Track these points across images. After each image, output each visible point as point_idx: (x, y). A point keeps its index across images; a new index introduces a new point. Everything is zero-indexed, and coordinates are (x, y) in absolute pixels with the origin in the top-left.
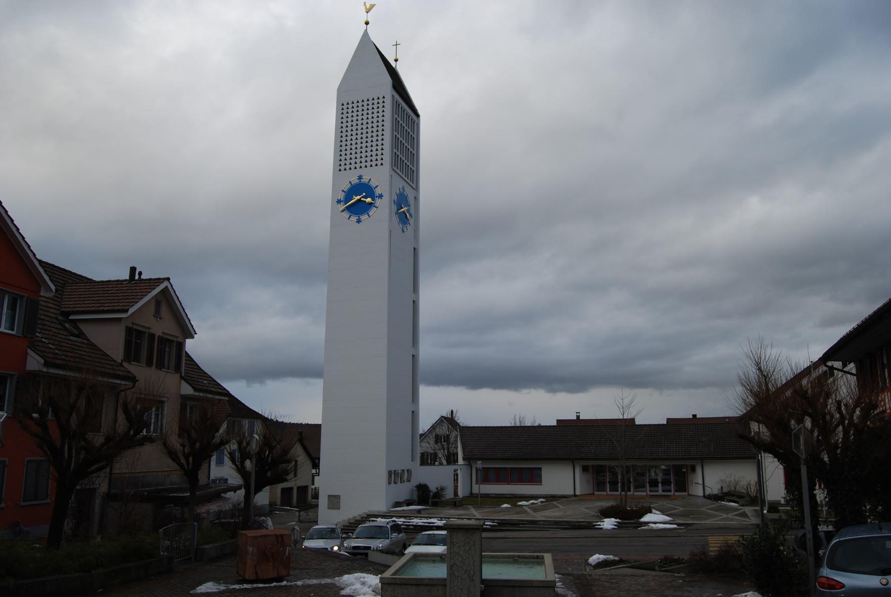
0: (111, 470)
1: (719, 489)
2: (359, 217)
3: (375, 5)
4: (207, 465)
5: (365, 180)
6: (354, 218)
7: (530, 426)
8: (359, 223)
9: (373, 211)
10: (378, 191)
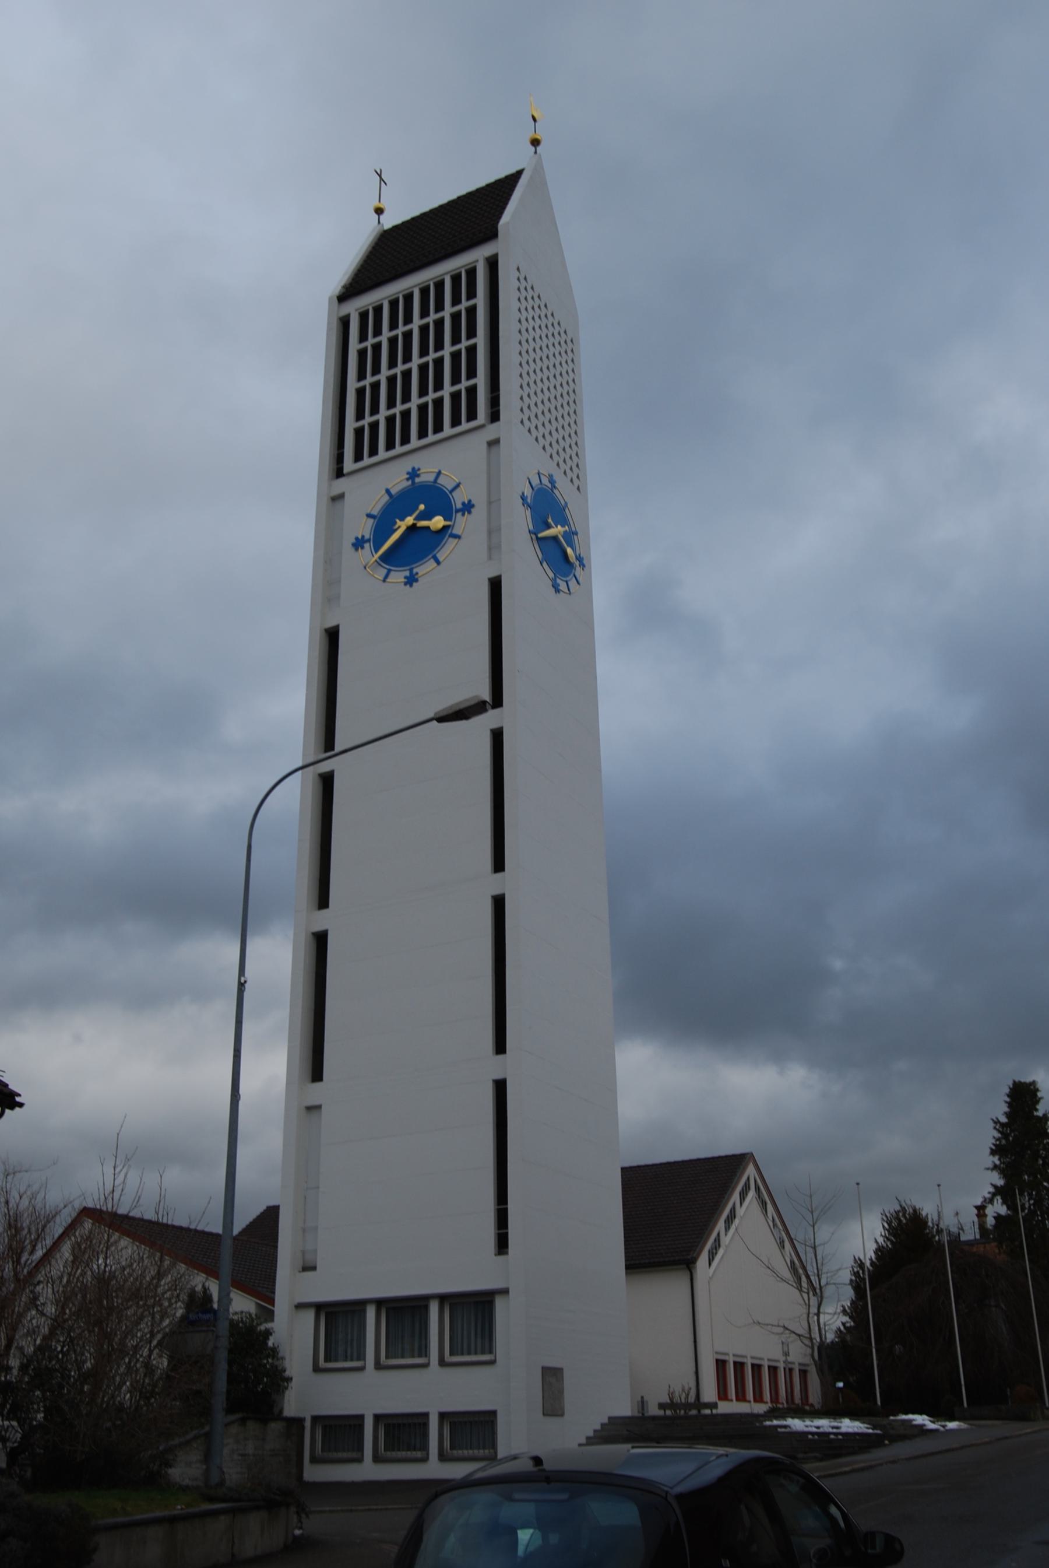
0: (6, 1450)
1: (638, 1402)
2: (411, 570)
3: (519, 174)
4: (529, 1550)
5: (426, 477)
6: (398, 576)
7: (181, 1228)
8: (411, 586)
9: (447, 550)
10: (459, 498)
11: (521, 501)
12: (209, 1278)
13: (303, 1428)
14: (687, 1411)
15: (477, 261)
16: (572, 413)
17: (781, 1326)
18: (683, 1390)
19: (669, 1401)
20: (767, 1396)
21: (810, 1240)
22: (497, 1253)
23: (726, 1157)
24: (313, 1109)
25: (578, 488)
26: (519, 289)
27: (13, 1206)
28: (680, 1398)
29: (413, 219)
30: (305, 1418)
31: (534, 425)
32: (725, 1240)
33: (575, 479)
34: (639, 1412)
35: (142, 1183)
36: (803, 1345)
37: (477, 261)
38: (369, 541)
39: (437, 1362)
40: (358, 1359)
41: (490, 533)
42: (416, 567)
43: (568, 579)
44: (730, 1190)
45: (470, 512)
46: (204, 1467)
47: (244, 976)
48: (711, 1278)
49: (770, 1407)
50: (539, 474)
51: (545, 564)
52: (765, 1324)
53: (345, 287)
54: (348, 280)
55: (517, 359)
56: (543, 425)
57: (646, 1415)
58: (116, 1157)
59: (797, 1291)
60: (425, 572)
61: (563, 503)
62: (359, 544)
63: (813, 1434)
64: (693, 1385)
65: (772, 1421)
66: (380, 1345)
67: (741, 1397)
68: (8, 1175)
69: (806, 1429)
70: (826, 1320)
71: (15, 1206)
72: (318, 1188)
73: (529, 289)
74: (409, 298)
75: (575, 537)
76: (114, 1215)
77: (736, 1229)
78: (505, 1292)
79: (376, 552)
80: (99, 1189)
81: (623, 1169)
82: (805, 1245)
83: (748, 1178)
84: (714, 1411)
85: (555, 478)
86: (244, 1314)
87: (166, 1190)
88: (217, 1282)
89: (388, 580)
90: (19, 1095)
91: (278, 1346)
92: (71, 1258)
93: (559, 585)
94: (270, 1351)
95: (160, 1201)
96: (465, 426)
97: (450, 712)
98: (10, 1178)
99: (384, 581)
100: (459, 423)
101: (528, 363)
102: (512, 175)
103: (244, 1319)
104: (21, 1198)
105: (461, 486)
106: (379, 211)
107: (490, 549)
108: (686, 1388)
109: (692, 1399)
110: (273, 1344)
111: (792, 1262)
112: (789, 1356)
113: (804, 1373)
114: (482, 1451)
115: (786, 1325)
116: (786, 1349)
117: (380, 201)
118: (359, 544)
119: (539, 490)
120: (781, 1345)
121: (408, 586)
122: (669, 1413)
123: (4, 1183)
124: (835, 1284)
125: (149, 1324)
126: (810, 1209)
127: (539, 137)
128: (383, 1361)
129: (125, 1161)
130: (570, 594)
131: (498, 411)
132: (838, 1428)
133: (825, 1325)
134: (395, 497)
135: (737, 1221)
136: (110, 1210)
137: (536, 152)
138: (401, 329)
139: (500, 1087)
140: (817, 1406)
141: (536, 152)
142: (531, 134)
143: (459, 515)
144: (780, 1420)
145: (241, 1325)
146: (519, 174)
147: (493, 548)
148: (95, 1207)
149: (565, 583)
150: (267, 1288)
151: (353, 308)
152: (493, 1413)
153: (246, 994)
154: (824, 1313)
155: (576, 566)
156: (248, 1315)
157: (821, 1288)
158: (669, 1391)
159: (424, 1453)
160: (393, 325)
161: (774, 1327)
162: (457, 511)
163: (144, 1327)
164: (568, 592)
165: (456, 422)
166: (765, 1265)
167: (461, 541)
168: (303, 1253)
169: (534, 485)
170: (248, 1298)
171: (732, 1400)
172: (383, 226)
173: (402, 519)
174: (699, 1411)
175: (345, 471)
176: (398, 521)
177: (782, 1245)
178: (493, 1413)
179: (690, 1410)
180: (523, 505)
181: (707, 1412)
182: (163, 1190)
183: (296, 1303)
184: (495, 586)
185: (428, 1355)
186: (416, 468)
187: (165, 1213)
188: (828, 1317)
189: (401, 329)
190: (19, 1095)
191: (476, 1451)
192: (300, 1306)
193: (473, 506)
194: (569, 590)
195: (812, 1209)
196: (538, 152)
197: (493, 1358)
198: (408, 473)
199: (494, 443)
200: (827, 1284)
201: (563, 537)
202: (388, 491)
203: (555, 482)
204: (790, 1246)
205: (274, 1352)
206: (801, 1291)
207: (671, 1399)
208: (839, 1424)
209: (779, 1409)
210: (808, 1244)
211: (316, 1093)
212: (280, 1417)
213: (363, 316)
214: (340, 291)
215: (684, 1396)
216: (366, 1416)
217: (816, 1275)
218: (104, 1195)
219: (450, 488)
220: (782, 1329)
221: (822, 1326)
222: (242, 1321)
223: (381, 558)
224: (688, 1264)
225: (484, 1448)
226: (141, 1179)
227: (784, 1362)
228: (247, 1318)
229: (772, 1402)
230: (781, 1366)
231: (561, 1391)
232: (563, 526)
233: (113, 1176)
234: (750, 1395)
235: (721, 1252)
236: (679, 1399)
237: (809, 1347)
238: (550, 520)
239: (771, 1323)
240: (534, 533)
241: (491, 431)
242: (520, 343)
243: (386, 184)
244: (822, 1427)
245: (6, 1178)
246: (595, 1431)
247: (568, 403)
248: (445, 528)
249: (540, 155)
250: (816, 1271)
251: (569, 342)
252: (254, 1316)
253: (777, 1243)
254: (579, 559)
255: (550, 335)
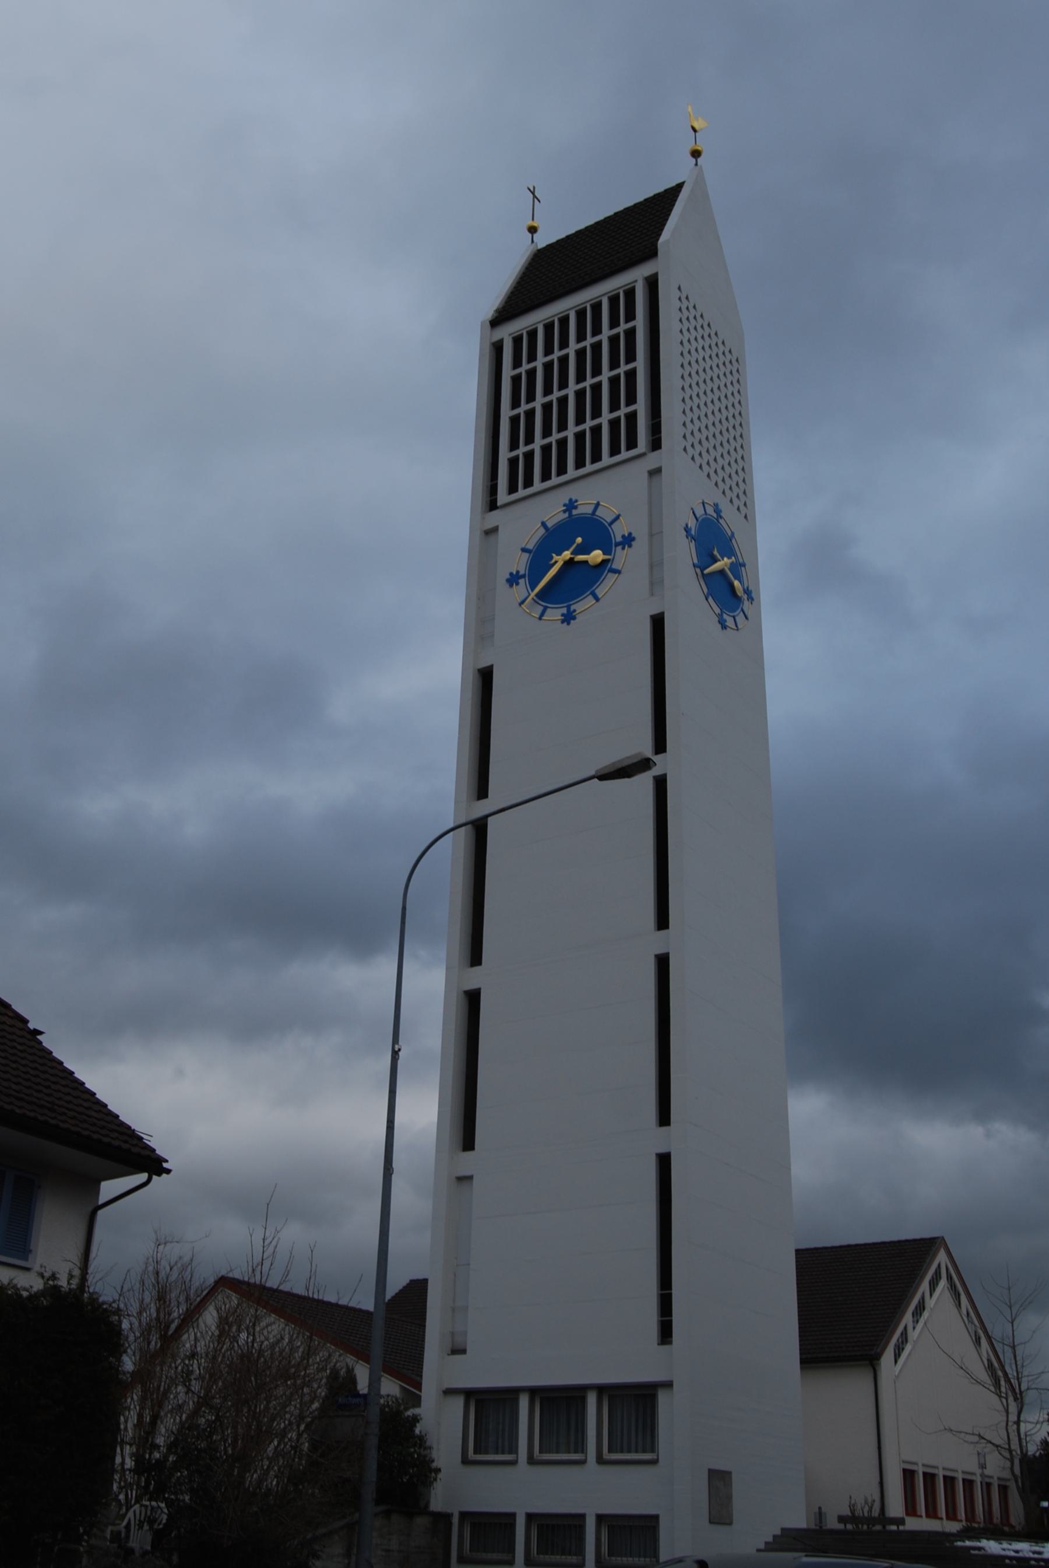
1: (815, 1513)
2: (568, 607)
3: (679, 187)
5: (584, 509)
6: (555, 614)
8: (568, 624)
9: (606, 586)
10: (618, 531)
11: (685, 533)
12: (360, 1361)
13: (451, 1524)
14: (870, 1526)
15: (636, 281)
16: (735, 382)
17: (976, 1435)
18: (866, 1502)
19: (850, 1514)
20: (962, 1513)
21: (1009, 1339)
22: (660, 1343)
23: (915, 1240)
24: (464, 1180)
25: (746, 517)
26: (680, 309)
27: (162, 1278)
28: (862, 1511)
29: (568, 237)
30: (452, 1514)
31: (698, 452)
32: (913, 1335)
33: (742, 508)
34: (816, 1525)
35: (292, 1256)
36: (1000, 1457)
37: (636, 281)
38: (523, 576)
39: (595, 1460)
40: (510, 1453)
41: (652, 567)
42: (574, 604)
43: (735, 614)
44: (919, 1278)
45: (630, 546)
46: (346, 1561)
47: (398, 1043)
48: (897, 1377)
49: (963, 1526)
50: (703, 503)
51: (710, 599)
52: (957, 1432)
53: (497, 311)
54: (500, 304)
55: (679, 407)
56: (708, 451)
57: (824, 1528)
58: (265, 1229)
59: (996, 1397)
60: (583, 609)
61: (730, 533)
62: (513, 580)
63: (1011, 1558)
64: (877, 1497)
65: (964, 1541)
66: (534, 1440)
67: (932, 1513)
68: (159, 1245)
69: (1003, 1553)
70: (1027, 1429)
71: (165, 1278)
72: (469, 1265)
73: (691, 308)
74: (564, 321)
75: (743, 568)
76: (263, 1288)
77: (925, 1323)
78: (668, 1385)
79: (532, 590)
80: (248, 1262)
81: (798, 1252)
82: (1004, 1344)
83: (939, 1265)
84: (901, 1528)
85: (721, 507)
86: (390, 1398)
87: (316, 1266)
88: (368, 1366)
89: (544, 618)
90: (167, 1161)
91: (426, 1435)
92: (217, 1333)
93: (726, 621)
94: (416, 1439)
95: (310, 1278)
96: (624, 455)
97: (612, 770)
98: (161, 1248)
99: (540, 618)
100: (619, 452)
101: (690, 363)
102: (672, 189)
103: (390, 1403)
104: (171, 1269)
105: (621, 518)
106: (533, 230)
107: (652, 584)
108: (870, 1501)
109: (876, 1513)
110: (420, 1432)
111: (989, 1360)
112: (986, 1468)
113: (1003, 1489)
114: (642, 1559)
115: (981, 1434)
116: (982, 1461)
117: (533, 219)
118: (513, 580)
119: (703, 520)
120: (976, 1457)
121: (565, 624)
122: (849, 1527)
123: (155, 1253)
124: (1037, 1389)
125: (298, 1406)
126: (1008, 1304)
127: (699, 148)
128: (537, 1456)
129: (275, 1233)
130: (738, 630)
131: (660, 439)
132: (1039, 1553)
133: (1026, 1436)
134: (551, 529)
135: (926, 1314)
136: (258, 1282)
137: (696, 164)
138: (557, 354)
139: (664, 1162)
140: (1018, 1528)
141: (696, 164)
142: (690, 146)
143: (619, 548)
144: (973, 1541)
145: (387, 1409)
146: (679, 187)
147: (655, 584)
148: (242, 1279)
149: (732, 619)
150: (413, 1370)
151: (506, 332)
152: (655, 1518)
153: (400, 1062)
154: (1025, 1422)
155: (744, 599)
156: (394, 1399)
157: (1021, 1393)
158: (850, 1503)
159: (580, 1558)
160: (549, 350)
161: (967, 1436)
162: (617, 544)
163: (293, 1408)
164: (735, 628)
165: (615, 450)
166: (958, 1365)
167: (621, 575)
168: (453, 1334)
169: (698, 516)
170: (387, 1378)
171: (921, 1516)
172: (537, 244)
173: (559, 554)
174: (884, 1527)
175: (499, 504)
176: (554, 555)
177: (977, 1341)
178: (655, 1518)
179: (874, 1525)
180: (687, 537)
181: (894, 1528)
182: (314, 1265)
183: (444, 1389)
184: (658, 623)
185: (585, 1452)
186: (574, 499)
187: (316, 1290)
188: (1029, 1426)
189: (557, 354)
190: (167, 1161)
191: (636, 1559)
192: (449, 1392)
193: (634, 539)
194: (736, 626)
195: (1010, 1303)
196: (699, 163)
197: (655, 1457)
198: (565, 505)
199: (655, 472)
200: (1028, 1389)
201: (729, 569)
202: (543, 524)
203: (721, 511)
204: (987, 1343)
205: (421, 1441)
206: (1000, 1397)
207: (853, 1512)
208: (1041, 1549)
209: (974, 1528)
210: (1005, 1342)
211: (467, 1163)
212: (425, 1511)
213: (517, 341)
214: (493, 315)
215: (866, 1509)
216: (517, 1515)
217: (1016, 1378)
218: (253, 1267)
219: (609, 520)
220: (976, 1439)
221: (1023, 1436)
222: (388, 1406)
223: (537, 595)
224: (872, 1361)
225: (645, 1557)
226: (291, 1254)
227: (981, 1475)
228: (393, 1402)
229: (967, 1520)
230: (978, 1479)
231: (730, 1497)
232: (729, 558)
233: (262, 1248)
234: (942, 1511)
235: (908, 1348)
236: (861, 1512)
237: (1008, 1459)
238: (716, 553)
239: (964, 1431)
240: (700, 566)
241: (653, 460)
242: (682, 366)
243: (539, 201)
244: (1021, 1551)
245: (158, 1248)
246: (775, 1536)
247: (732, 383)
248: (604, 562)
249: (701, 166)
250: (1015, 1374)
251: (734, 361)
252: (400, 1401)
253: (973, 1341)
254: (747, 592)
255: (714, 356)
